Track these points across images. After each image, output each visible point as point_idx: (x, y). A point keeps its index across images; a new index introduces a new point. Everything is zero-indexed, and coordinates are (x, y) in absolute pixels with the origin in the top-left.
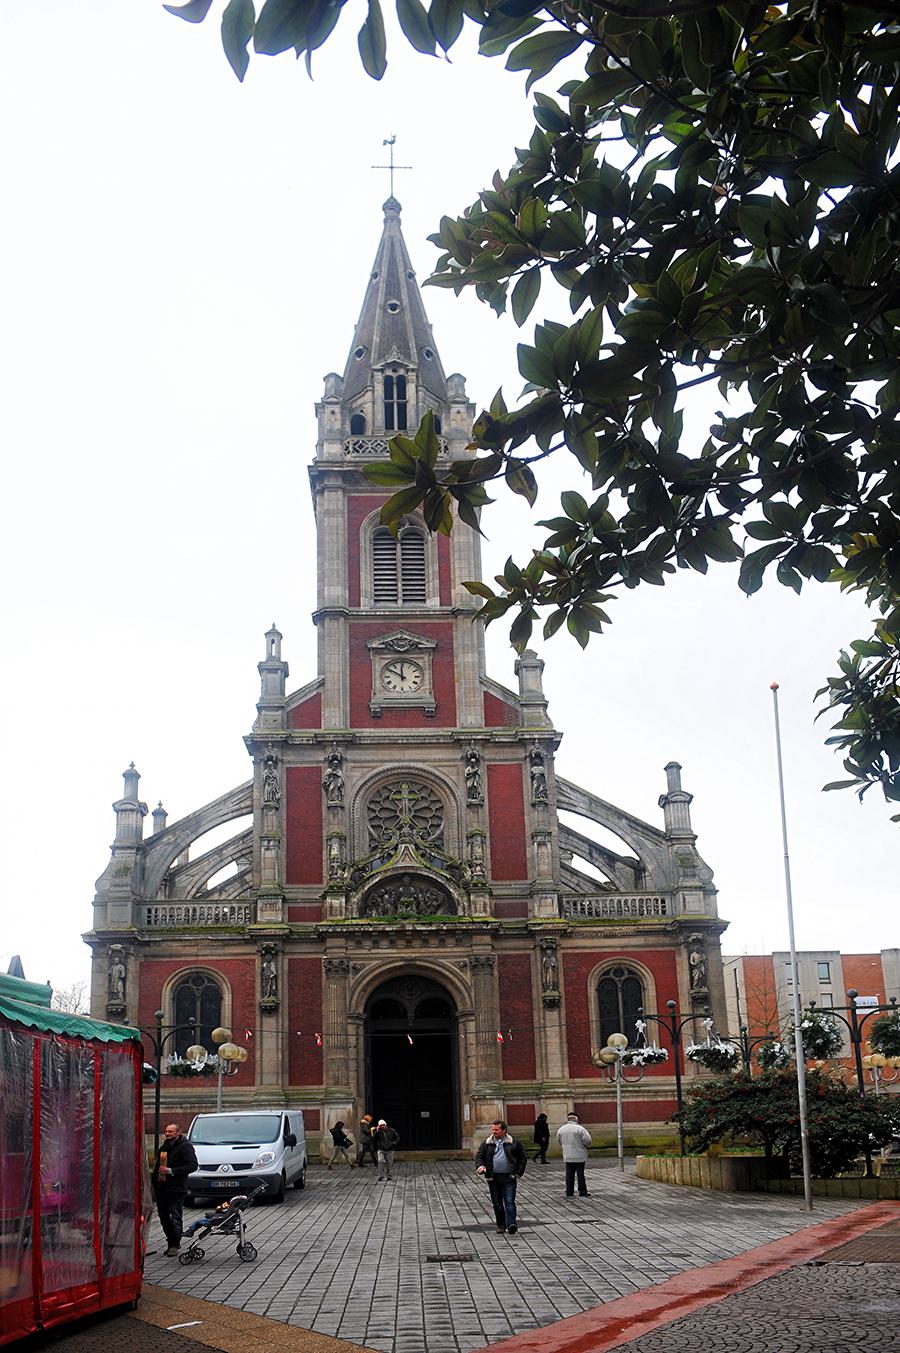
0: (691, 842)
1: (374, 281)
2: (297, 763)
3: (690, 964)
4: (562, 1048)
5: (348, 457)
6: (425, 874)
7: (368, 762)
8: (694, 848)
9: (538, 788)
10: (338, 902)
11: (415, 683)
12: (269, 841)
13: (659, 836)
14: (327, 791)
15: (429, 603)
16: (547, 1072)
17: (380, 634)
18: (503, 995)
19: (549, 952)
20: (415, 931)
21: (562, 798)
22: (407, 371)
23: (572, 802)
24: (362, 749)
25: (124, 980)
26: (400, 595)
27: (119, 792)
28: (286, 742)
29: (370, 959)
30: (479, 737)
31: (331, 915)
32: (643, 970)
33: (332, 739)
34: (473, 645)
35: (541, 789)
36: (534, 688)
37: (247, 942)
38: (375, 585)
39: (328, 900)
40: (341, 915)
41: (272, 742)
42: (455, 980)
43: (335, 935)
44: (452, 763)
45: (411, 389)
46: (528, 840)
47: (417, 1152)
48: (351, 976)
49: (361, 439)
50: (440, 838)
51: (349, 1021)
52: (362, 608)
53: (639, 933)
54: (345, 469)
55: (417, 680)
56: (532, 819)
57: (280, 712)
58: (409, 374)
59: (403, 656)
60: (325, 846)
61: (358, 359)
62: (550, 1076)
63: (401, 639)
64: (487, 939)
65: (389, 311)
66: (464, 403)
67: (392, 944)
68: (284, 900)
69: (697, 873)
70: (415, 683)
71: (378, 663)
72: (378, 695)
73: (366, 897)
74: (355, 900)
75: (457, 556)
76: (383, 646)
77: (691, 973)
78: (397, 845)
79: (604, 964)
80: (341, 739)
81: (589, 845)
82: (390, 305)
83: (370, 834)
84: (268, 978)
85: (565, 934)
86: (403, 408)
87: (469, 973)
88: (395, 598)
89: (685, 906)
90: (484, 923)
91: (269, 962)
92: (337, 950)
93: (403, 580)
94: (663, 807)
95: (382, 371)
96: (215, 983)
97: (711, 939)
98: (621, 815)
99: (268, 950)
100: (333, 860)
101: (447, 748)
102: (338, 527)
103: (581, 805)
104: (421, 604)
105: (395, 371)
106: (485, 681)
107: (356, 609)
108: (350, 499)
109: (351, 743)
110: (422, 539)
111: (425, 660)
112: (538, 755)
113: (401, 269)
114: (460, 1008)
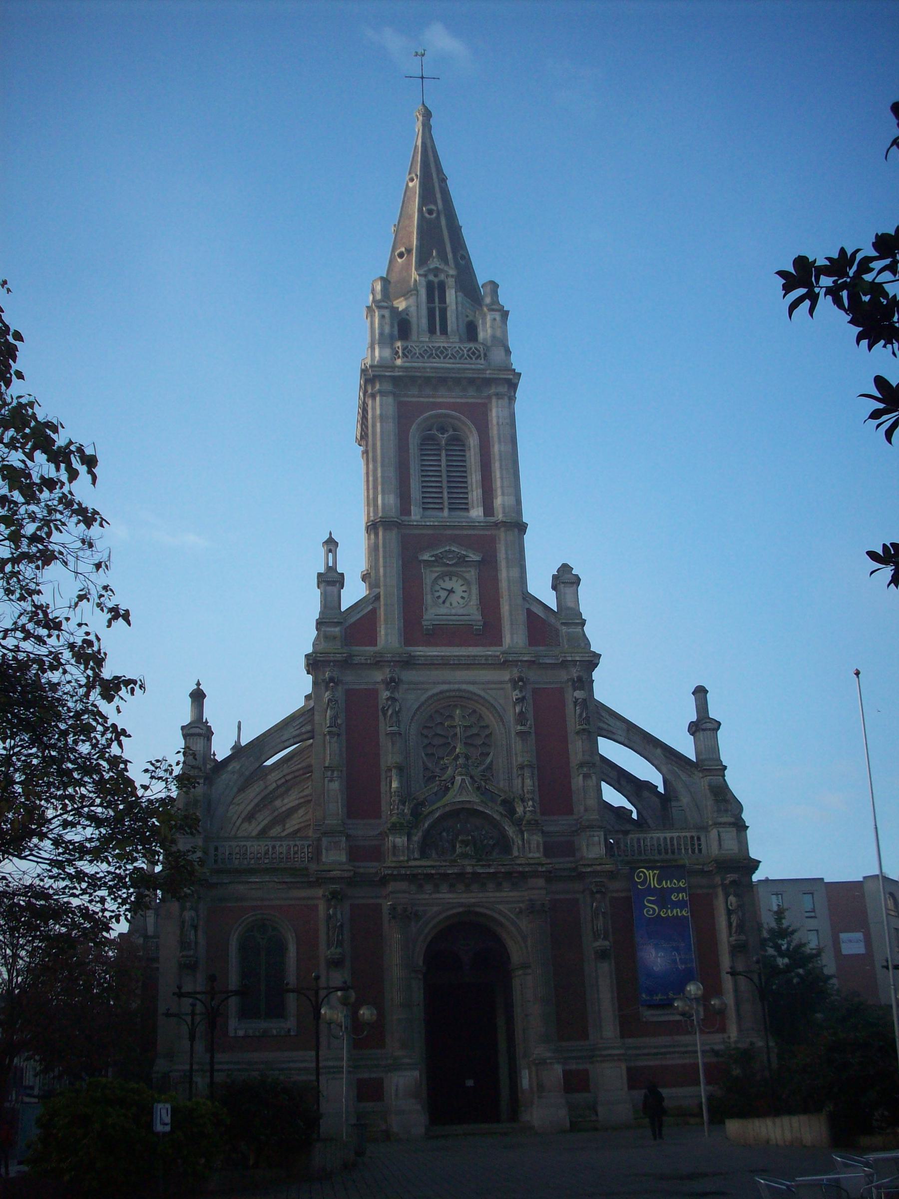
5: (399, 362)
6: (481, 809)
9: (581, 715)
11: (463, 598)
12: (333, 771)
14: (385, 714)
19: (598, 896)
20: (474, 874)
21: (602, 725)
22: (447, 276)
23: (611, 729)
25: (195, 927)
26: (446, 504)
27: (186, 717)
33: (389, 659)
35: (584, 715)
38: (423, 492)
49: (409, 344)
50: (490, 767)
52: (413, 518)
54: (397, 374)
55: (465, 595)
56: (577, 749)
59: (451, 569)
63: (450, 551)
64: (541, 882)
68: (348, 837)
69: (730, 808)
70: (463, 598)
71: (429, 577)
73: (427, 835)
76: (433, 559)
77: (729, 918)
86: (443, 312)
89: (720, 845)
90: (539, 864)
105: (436, 276)
106: (528, 598)
107: (406, 518)
109: (408, 663)
110: (464, 445)
111: (472, 574)
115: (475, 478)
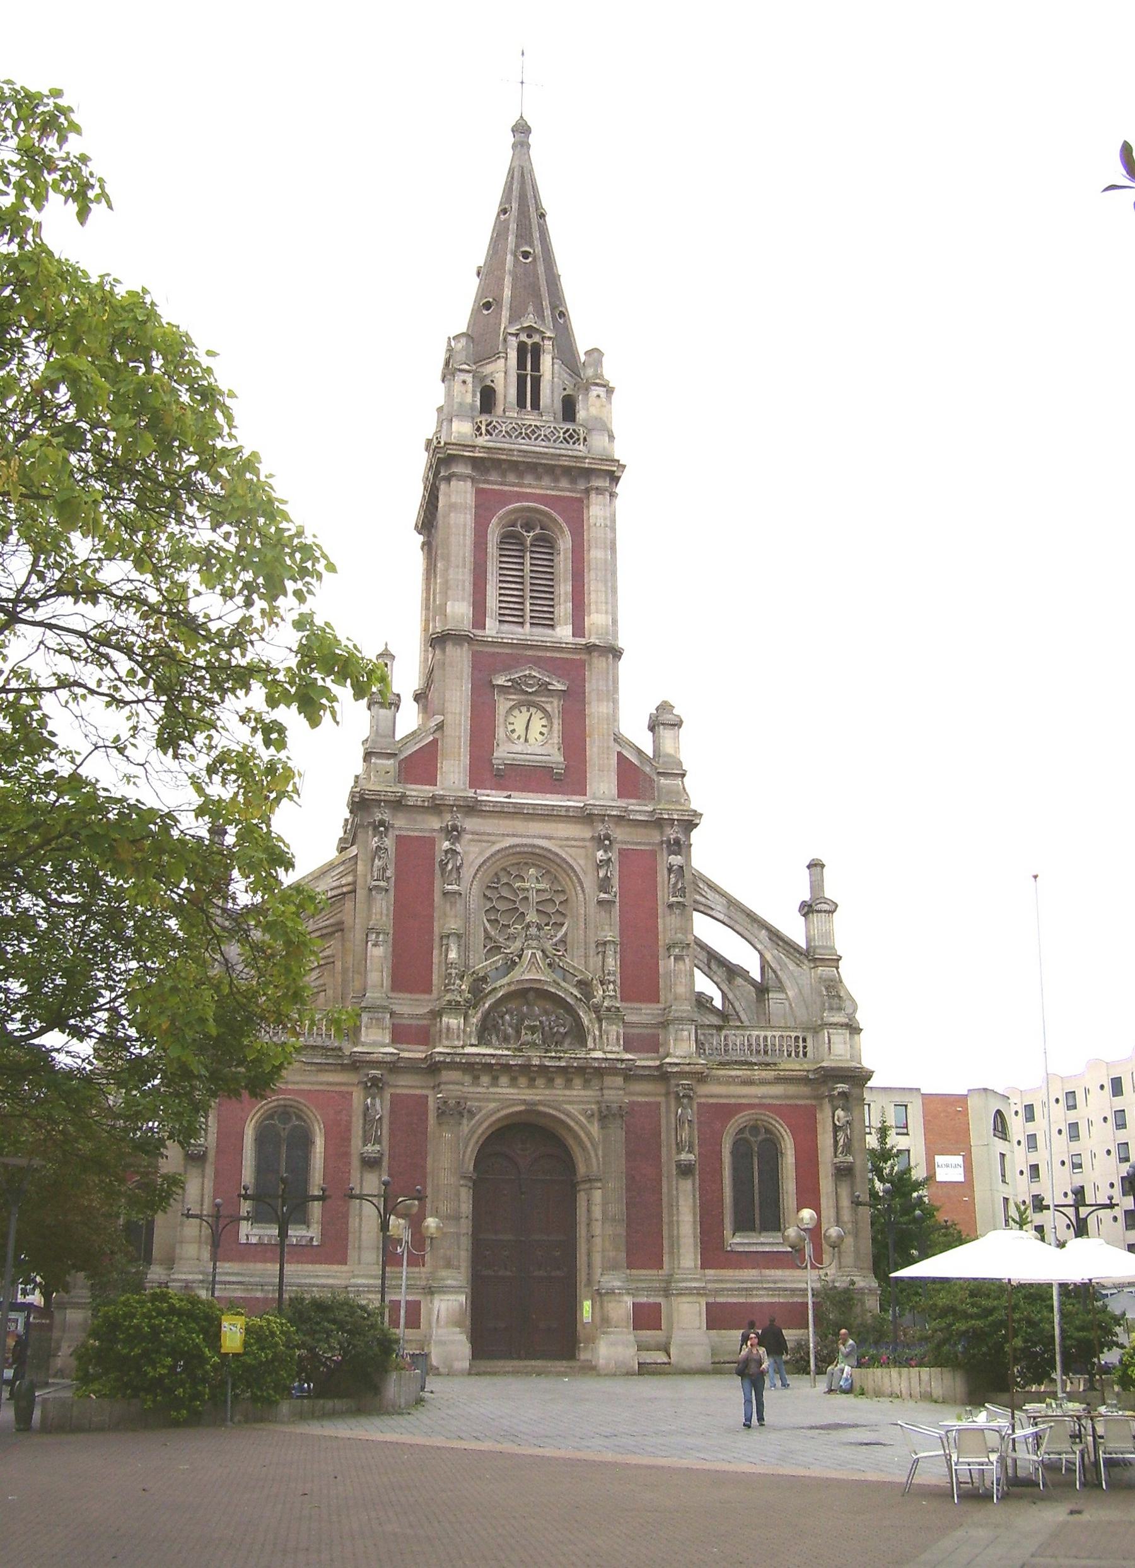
0: (836, 964)
1: (502, 217)
2: (408, 829)
3: (834, 1124)
4: (695, 1228)
5: (481, 441)
6: (553, 990)
7: (489, 834)
8: (838, 972)
10: (453, 1021)
12: (378, 934)
13: (801, 954)
15: (559, 630)
16: (679, 1260)
17: (506, 668)
18: (630, 1155)
19: (685, 1101)
22: (543, 338)
24: (482, 817)
26: (528, 619)
28: (399, 802)
29: (488, 1100)
30: (614, 813)
31: (447, 1038)
32: (784, 1133)
33: (451, 803)
34: (608, 691)
35: (680, 886)
36: (671, 751)
37: (344, 1068)
39: (445, 1019)
40: (459, 1040)
41: (384, 801)
42: (582, 1135)
43: (452, 1066)
44: (581, 844)
45: (546, 361)
46: (662, 951)
47: (533, 1363)
48: (465, 1121)
50: (563, 941)
51: (462, 1182)
52: (487, 632)
53: (779, 1080)
54: (476, 455)
55: (544, 730)
56: (667, 924)
57: (392, 761)
58: (546, 342)
60: (436, 944)
61: (486, 312)
62: (681, 1266)
63: (531, 677)
64: (619, 1080)
65: (521, 258)
66: (604, 386)
67: (513, 1082)
68: (392, 1014)
70: (542, 734)
71: (503, 705)
72: (501, 749)
73: (486, 1016)
74: (475, 1020)
75: (593, 574)
76: (510, 684)
77: (835, 1136)
78: (522, 950)
79: (739, 1120)
80: (462, 803)
81: (708, 953)
82: (523, 252)
83: (485, 930)
84: (372, 1121)
85: (701, 1078)
86: (536, 382)
87: (596, 1124)
88: (521, 620)
91: (373, 1098)
92: (456, 1085)
93: (531, 597)
94: (804, 915)
95: (517, 335)
96: (304, 1121)
97: (856, 1091)
98: (753, 918)
99: (375, 1081)
100: (449, 965)
101: (575, 823)
102: (465, 525)
103: (719, 908)
104: (549, 631)
105: (529, 336)
106: (618, 739)
108: (479, 492)
109: (472, 808)
110: (552, 547)
111: (553, 706)
112: (677, 842)
113: (532, 209)
114: (582, 1169)
115: (564, 588)
